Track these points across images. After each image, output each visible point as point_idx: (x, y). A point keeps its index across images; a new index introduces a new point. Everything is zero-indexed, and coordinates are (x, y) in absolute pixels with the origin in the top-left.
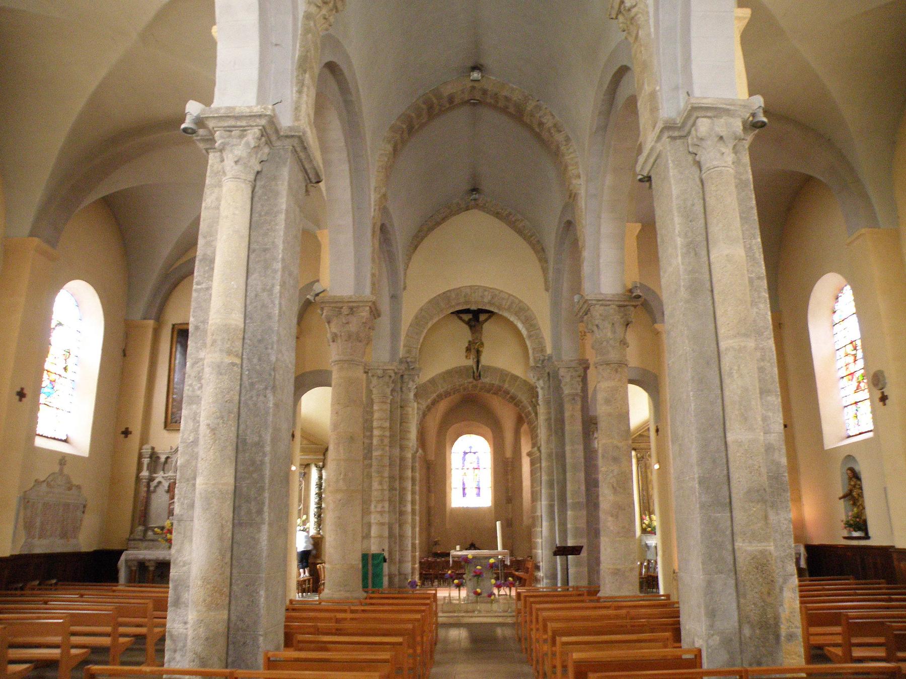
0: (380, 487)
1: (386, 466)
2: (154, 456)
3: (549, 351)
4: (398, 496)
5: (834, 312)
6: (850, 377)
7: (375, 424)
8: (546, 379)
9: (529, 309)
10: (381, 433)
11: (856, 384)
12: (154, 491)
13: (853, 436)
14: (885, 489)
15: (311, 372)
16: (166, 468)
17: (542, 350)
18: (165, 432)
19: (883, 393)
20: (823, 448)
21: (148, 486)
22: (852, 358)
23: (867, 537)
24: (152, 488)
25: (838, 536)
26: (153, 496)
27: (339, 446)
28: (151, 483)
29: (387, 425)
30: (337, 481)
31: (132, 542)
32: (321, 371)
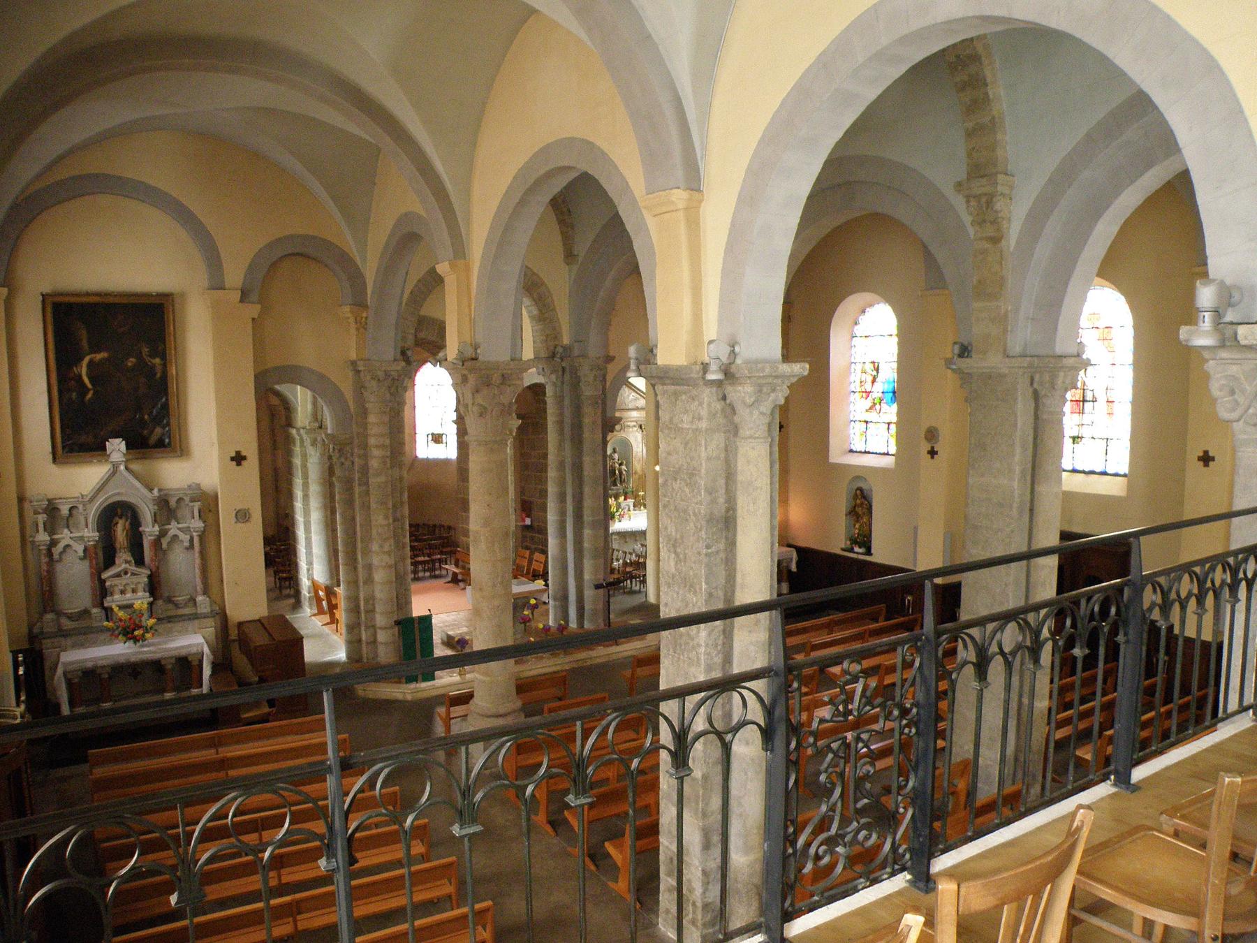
0: (386, 523)
1: (525, 558)
2: (51, 509)
3: (566, 340)
4: (1211, 872)
5: (856, 324)
6: (864, 395)
7: (372, 441)
8: (560, 373)
9: (543, 283)
10: (383, 453)
11: (871, 404)
12: (60, 560)
13: (856, 452)
14: (916, 528)
15: (277, 368)
16: (71, 522)
17: (556, 337)
18: (53, 466)
19: (933, 448)
20: (827, 456)
21: (50, 554)
22: (871, 378)
23: (869, 552)
24: (56, 557)
25: (836, 542)
26: (59, 568)
27: (494, 545)
28: (54, 550)
29: (387, 442)
30: (494, 586)
31: (48, 641)
32: (296, 366)
